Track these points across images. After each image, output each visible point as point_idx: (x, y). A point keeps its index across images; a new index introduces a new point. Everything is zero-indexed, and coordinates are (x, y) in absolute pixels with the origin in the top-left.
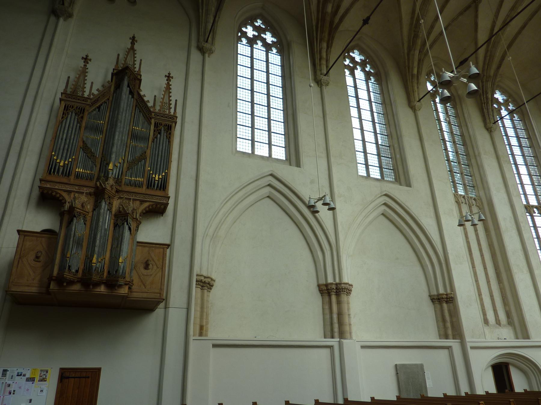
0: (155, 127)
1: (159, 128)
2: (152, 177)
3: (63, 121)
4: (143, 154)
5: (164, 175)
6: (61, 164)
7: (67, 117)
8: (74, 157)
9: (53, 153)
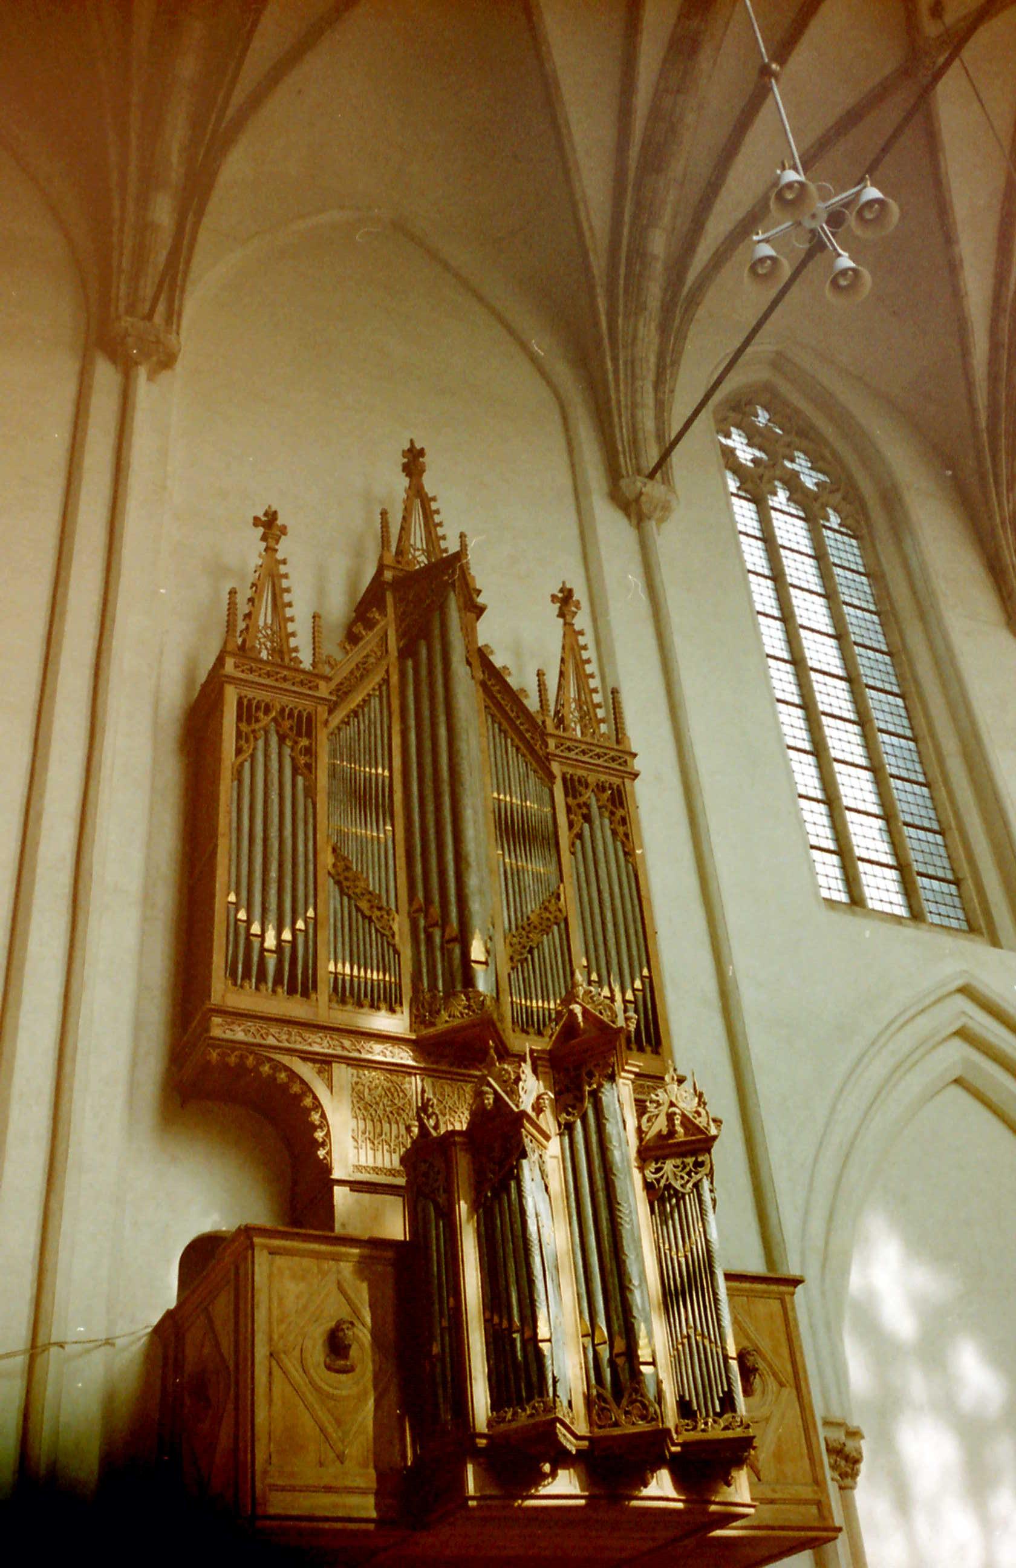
0: (566, 795)
1: (581, 800)
3: (242, 765)
5: (245, 918)
6: (270, 942)
7: (255, 749)
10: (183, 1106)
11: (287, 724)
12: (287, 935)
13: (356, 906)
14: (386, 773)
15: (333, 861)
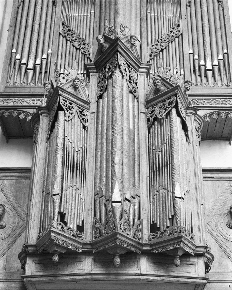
4: (174, 28)
5: (222, 58)
8: (50, 51)
9: (14, 51)
10: (7, 142)
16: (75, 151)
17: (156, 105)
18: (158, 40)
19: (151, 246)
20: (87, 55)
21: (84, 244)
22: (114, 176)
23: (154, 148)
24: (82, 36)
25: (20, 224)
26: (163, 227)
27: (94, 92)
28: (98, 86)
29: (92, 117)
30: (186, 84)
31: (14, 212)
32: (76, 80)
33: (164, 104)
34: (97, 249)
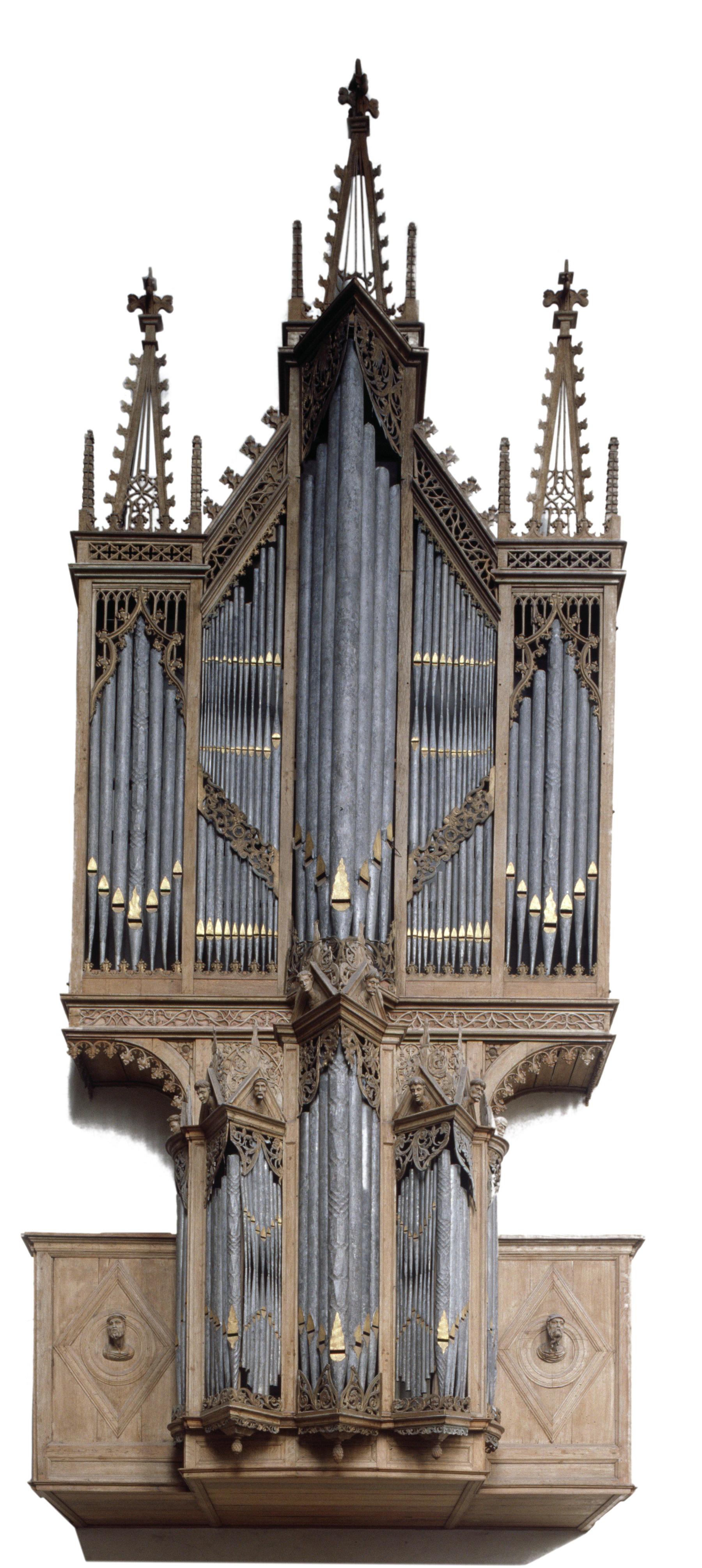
1: (536, 636)
2: (528, 911)
3: (103, 690)
4: (473, 795)
6: (135, 911)
7: (118, 664)
8: (178, 868)
10: (91, 1096)
11: (155, 618)
12: (152, 900)
13: (232, 849)
14: (278, 660)
15: (205, 795)
16: (260, 1237)
17: (413, 1132)
18: (436, 834)
19: (395, 1422)
20: (266, 881)
21: (282, 1419)
22: (333, 1301)
23: (406, 1228)
24: (254, 823)
25: (160, 1351)
26: (417, 1391)
27: (293, 1091)
28: (300, 1079)
29: (291, 1155)
30: (474, 1088)
31: (147, 1327)
32: (259, 1083)
33: (428, 1136)
34: (304, 1429)
